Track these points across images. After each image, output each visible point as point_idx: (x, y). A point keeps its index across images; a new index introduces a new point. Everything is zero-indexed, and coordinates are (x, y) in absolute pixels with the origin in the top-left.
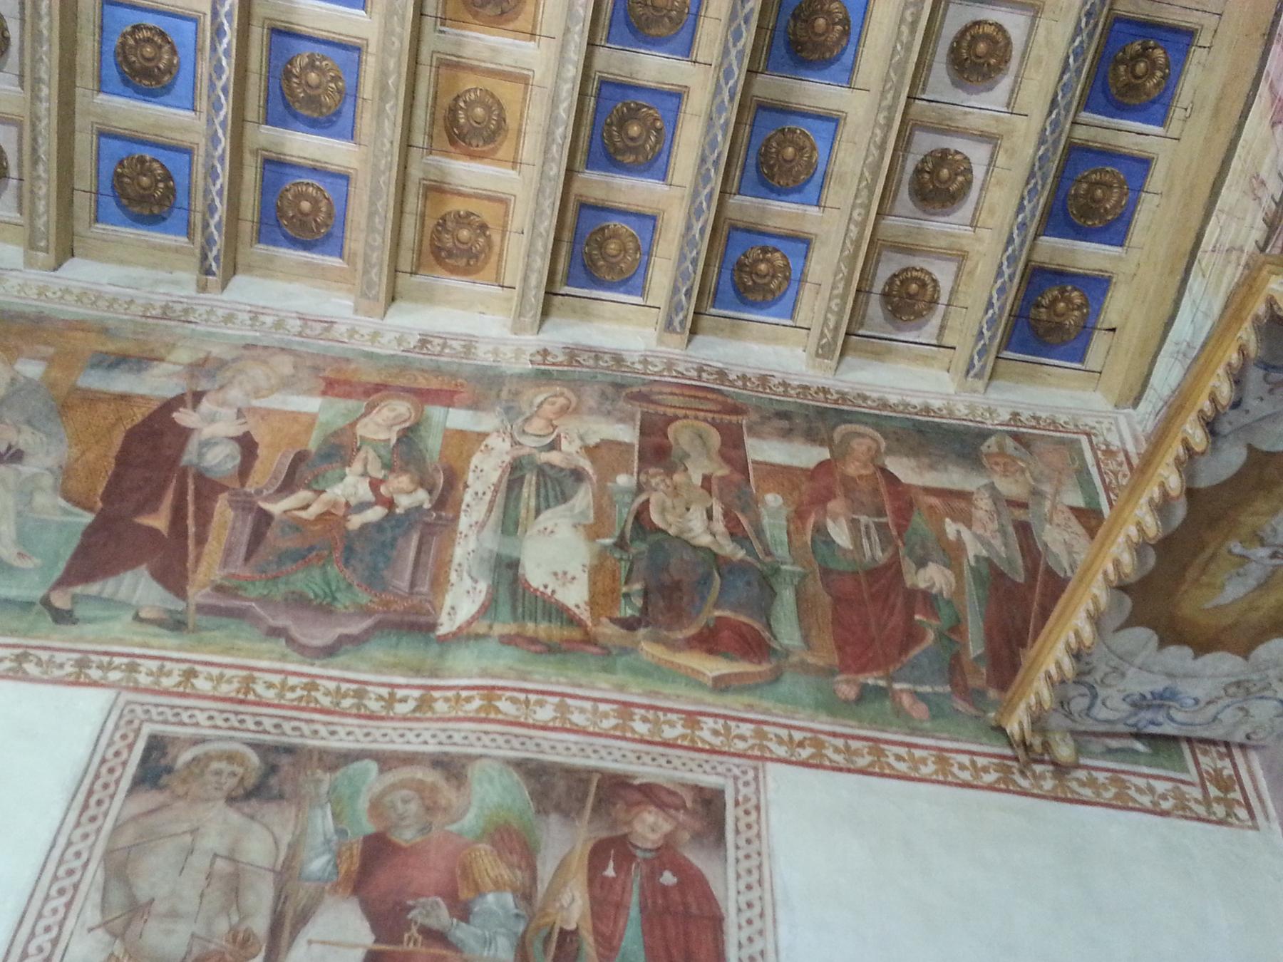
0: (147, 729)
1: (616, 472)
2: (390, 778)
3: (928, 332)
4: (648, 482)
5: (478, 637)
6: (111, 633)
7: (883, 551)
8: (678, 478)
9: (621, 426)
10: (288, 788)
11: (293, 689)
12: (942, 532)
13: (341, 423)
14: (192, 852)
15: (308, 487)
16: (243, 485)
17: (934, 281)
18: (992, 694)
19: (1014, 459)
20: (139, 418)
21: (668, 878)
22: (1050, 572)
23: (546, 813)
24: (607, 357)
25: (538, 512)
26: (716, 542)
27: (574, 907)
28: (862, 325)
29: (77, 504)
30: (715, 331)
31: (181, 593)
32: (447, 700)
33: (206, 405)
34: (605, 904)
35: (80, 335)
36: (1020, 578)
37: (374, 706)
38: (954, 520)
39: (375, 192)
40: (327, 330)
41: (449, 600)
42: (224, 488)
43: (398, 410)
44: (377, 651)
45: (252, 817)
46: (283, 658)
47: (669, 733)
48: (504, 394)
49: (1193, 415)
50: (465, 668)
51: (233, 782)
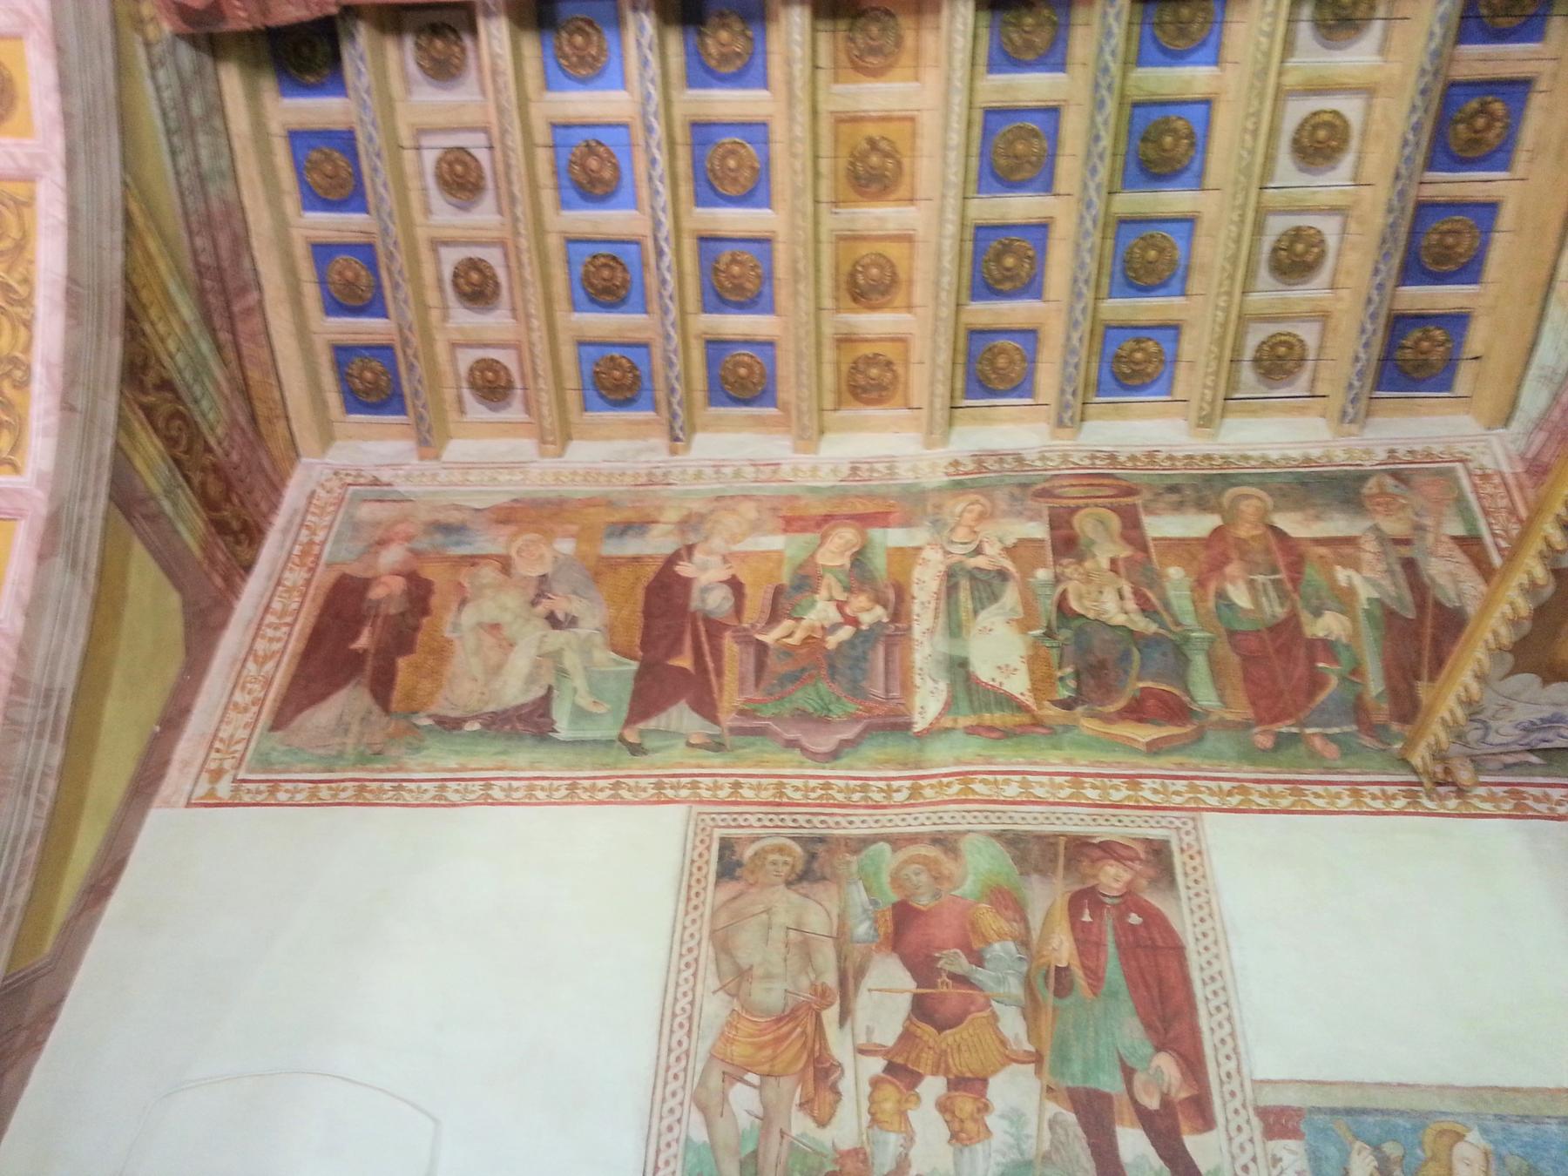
0: (718, 833)
1: (1034, 567)
2: (903, 854)
3: (1301, 385)
4: (1063, 574)
5: (947, 730)
6: (673, 758)
7: (1282, 605)
8: (1088, 564)
9: (1032, 524)
10: (828, 871)
11: (813, 790)
12: (1332, 580)
13: (803, 555)
14: (770, 927)
15: (790, 617)
16: (740, 621)
17: (1301, 341)
18: (1395, 727)
19: (1394, 496)
20: (651, 576)
21: (1134, 919)
22: (1438, 605)
23: (1028, 874)
24: (1009, 459)
25: (976, 613)
26: (1131, 620)
27: (1062, 949)
28: (1236, 390)
29: (625, 655)
30: (1099, 416)
31: (714, 720)
32: (932, 786)
33: (698, 556)
34: (1087, 943)
35: (592, 510)
36: (1411, 615)
37: (878, 797)
38: (1344, 566)
39: (799, 355)
40: (774, 472)
41: (918, 701)
42: (726, 627)
43: (844, 537)
44: (869, 751)
45: (806, 896)
46: (801, 765)
47: (1116, 796)
48: (930, 509)
49: (1551, 518)
50: (943, 756)
51: (786, 869)
